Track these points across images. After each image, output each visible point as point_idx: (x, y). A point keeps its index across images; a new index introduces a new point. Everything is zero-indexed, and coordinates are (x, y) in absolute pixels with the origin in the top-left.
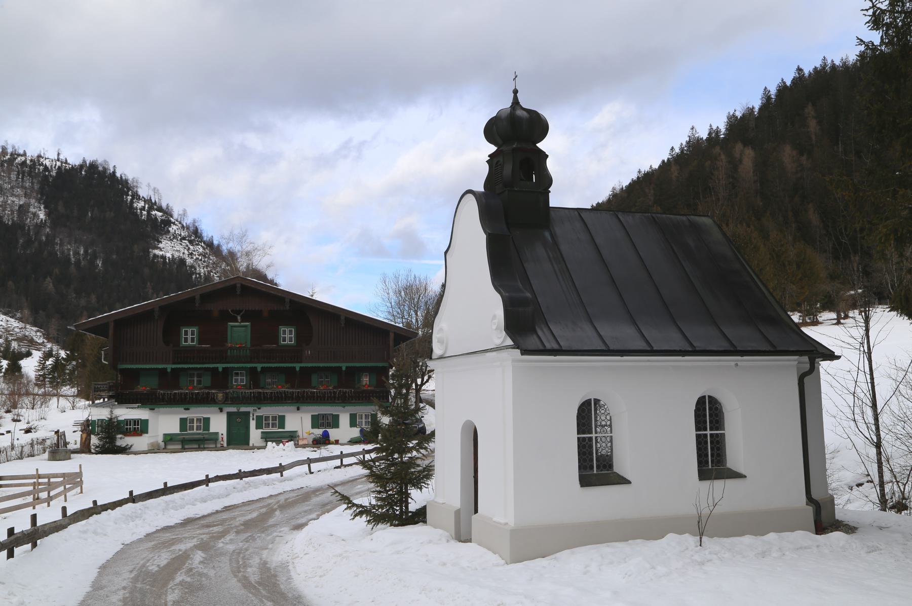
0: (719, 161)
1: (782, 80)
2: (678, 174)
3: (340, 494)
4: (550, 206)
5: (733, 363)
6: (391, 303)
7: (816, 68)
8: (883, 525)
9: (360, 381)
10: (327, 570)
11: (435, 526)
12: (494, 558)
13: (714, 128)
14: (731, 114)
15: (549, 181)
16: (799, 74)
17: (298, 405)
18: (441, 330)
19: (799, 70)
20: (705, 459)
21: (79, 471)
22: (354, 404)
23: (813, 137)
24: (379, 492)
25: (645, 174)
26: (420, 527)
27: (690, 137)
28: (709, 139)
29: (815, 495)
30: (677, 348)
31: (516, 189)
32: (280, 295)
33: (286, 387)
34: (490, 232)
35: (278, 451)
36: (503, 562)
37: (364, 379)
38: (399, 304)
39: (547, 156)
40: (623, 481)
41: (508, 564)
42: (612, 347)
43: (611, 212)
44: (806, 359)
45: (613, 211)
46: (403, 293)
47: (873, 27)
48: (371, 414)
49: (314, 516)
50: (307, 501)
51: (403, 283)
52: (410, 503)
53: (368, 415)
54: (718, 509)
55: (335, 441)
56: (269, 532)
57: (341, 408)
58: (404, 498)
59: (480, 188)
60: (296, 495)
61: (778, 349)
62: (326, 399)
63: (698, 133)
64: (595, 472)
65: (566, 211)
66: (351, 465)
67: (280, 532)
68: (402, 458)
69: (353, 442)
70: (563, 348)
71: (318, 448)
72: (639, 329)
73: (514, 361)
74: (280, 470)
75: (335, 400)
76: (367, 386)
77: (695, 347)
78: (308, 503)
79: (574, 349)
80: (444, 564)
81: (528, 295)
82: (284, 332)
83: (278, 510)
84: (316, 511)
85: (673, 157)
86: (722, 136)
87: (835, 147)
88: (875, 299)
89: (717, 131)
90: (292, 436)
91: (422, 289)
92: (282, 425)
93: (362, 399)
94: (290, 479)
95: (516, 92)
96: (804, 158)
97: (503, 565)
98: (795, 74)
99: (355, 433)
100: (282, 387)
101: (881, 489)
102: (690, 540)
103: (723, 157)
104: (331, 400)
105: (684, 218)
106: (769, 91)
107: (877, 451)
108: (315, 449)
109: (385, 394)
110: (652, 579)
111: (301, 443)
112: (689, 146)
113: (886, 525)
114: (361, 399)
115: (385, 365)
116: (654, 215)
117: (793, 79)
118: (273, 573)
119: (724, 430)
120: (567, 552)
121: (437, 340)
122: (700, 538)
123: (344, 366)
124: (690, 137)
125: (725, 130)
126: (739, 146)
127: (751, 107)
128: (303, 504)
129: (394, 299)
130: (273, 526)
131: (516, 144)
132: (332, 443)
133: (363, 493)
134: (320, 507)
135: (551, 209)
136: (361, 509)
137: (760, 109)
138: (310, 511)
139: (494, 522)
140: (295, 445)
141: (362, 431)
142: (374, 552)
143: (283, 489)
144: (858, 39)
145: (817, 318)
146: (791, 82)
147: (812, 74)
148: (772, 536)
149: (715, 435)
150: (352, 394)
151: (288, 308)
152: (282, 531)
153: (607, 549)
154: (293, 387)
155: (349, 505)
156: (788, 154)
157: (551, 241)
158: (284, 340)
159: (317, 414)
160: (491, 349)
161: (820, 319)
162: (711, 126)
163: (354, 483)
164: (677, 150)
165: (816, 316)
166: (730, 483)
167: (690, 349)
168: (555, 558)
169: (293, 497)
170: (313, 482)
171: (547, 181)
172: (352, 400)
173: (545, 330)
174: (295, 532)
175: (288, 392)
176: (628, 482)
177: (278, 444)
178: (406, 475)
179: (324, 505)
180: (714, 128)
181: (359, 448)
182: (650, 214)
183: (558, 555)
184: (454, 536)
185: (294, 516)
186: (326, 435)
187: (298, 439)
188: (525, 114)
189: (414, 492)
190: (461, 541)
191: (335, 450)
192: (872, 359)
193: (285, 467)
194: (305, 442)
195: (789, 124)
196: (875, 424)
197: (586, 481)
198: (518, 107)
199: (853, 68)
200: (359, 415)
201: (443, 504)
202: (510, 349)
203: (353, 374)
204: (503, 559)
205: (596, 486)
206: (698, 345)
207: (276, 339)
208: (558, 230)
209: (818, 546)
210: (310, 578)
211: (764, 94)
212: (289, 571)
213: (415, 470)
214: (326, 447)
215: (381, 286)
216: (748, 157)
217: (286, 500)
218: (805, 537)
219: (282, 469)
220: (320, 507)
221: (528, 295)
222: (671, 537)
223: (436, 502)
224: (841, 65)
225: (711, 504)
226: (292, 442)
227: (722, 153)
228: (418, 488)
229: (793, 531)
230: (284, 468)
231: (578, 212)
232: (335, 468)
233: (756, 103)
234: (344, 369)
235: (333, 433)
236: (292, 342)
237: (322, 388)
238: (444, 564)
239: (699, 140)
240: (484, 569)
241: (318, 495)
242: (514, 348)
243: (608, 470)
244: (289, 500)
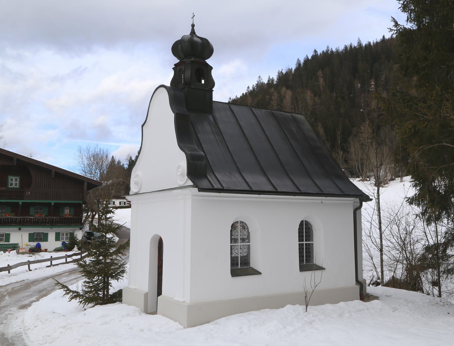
0: (273, 96)
1: (307, 56)
2: (252, 101)
3: (61, 284)
4: (213, 100)
5: (320, 201)
6: (84, 165)
7: (323, 51)
8: (388, 295)
9: (63, 212)
10: (55, 338)
11: (129, 305)
12: (176, 325)
13: (271, 78)
14: (280, 71)
15: (213, 84)
16: (315, 53)
17: (19, 227)
18: (137, 176)
19: (315, 51)
20: (302, 259)
22: (59, 226)
23: (321, 87)
24: (88, 283)
25: (233, 100)
26: (118, 305)
27: (258, 82)
28: (268, 84)
29: (360, 279)
30: (291, 191)
31: (192, 87)
32: (10, 155)
33: (12, 215)
34: (177, 112)
35: (5, 256)
36: (182, 327)
37: (66, 211)
38: (89, 165)
39: (212, 68)
40: (256, 273)
41: (185, 329)
42: (254, 189)
43: (248, 107)
44: (358, 200)
45: (249, 107)
46: (92, 159)
47: (403, 10)
48: (70, 233)
49: (34, 299)
50: (28, 289)
51: (92, 152)
52: (110, 289)
53: (68, 233)
54: (319, 288)
55: (45, 249)
56: (2, 311)
57: (49, 229)
58: (106, 285)
59: (168, 84)
60: (20, 285)
61: (345, 193)
62: (32, 222)
63: (262, 80)
64: (239, 267)
65: (221, 104)
66: (57, 265)
67: (10, 311)
68: (105, 260)
69: (57, 250)
70: (225, 188)
71: (33, 254)
72: (268, 178)
73: (193, 195)
74: (8, 269)
75: (46, 224)
76: (68, 215)
77: (301, 191)
78: (29, 290)
79: (231, 189)
80: (142, 330)
81: (202, 153)
82: (12, 180)
83: (7, 296)
84: (35, 296)
85: (249, 92)
86: (275, 83)
87: (332, 94)
88: (350, 175)
89: (273, 80)
90: (15, 247)
91: (105, 157)
92: (8, 239)
93: (65, 224)
94: (15, 275)
95: (193, 26)
96: (317, 98)
97: (182, 329)
98: (313, 53)
99: (59, 244)
100: (9, 215)
101: (382, 274)
102: (300, 308)
103: (275, 94)
104: (43, 224)
105: (289, 114)
106: (300, 61)
107: (381, 253)
108: (31, 255)
109: (80, 220)
110: (286, 335)
111: (20, 251)
112: (257, 87)
113: (390, 294)
114: (63, 223)
115: (81, 203)
116: (272, 111)
117: (312, 56)
118: (10, 342)
119: (313, 241)
120: (224, 319)
121: (134, 183)
122: (306, 307)
123: (53, 202)
124: (258, 82)
125: (276, 79)
126: (284, 89)
127: (291, 69)
128: (25, 291)
129: (86, 162)
130: (5, 307)
131: (193, 58)
132: (43, 251)
133: (67, 283)
134: (37, 292)
135: (213, 102)
136: (76, 294)
137: (295, 70)
138: (31, 296)
139: (175, 300)
140: (17, 252)
141: (64, 243)
142: (89, 323)
143: (10, 281)
144: (392, 18)
146: (311, 57)
147: (321, 54)
148: (342, 304)
149: (308, 244)
150: (57, 220)
151: (15, 164)
152: (12, 310)
153: (253, 315)
154: (16, 215)
155: (67, 292)
156: (309, 95)
157: (213, 120)
158: (11, 184)
159: (33, 232)
160: (176, 188)
162: (269, 77)
163: (60, 276)
164: (251, 88)
166: (318, 273)
167: (298, 192)
168: (217, 323)
169: (17, 287)
170: (31, 276)
171: (211, 84)
172: (58, 224)
173: (212, 176)
174: (22, 310)
175: (13, 218)
176: (260, 273)
177: (5, 252)
178: (108, 271)
179: (40, 291)
180: (271, 78)
181: (63, 254)
182: (270, 110)
183: (218, 321)
184: (143, 310)
185: (19, 300)
186: (39, 246)
187: (18, 248)
188: (199, 40)
189: (113, 282)
190: (147, 313)
191: (46, 256)
192: (380, 202)
193: (12, 267)
194: (24, 251)
195: (310, 79)
196: (380, 239)
197: (235, 273)
198: (194, 35)
199: (341, 53)
200: (62, 233)
201: (135, 289)
202: (191, 188)
203: (58, 208)
204: (181, 325)
206: (303, 189)
207: (5, 183)
208: (217, 115)
209: (368, 309)
210: (42, 344)
211: (297, 62)
212: (23, 340)
213: (115, 267)
214: (39, 254)
215: (77, 154)
216: (288, 94)
217: (13, 288)
218: (358, 303)
219: (10, 269)
220: (37, 292)
221: (202, 153)
222: (288, 307)
223: (129, 288)
224: (336, 51)
225: (313, 286)
226: (15, 251)
227: (275, 92)
228: (116, 279)
229: (352, 300)
230: (11, 268)
231: (229, 106)
232: (46, 267)
233: (293, 67)
234: (53, 204)
235: (44, 245)
236: (17, 186)
237: (37, 216)
238: (142, 330)
239: (263, 84)
240: (170, 333)
241: (35, 285)
242: (194, 187)
243: (247, 266)
244: (15, 289)
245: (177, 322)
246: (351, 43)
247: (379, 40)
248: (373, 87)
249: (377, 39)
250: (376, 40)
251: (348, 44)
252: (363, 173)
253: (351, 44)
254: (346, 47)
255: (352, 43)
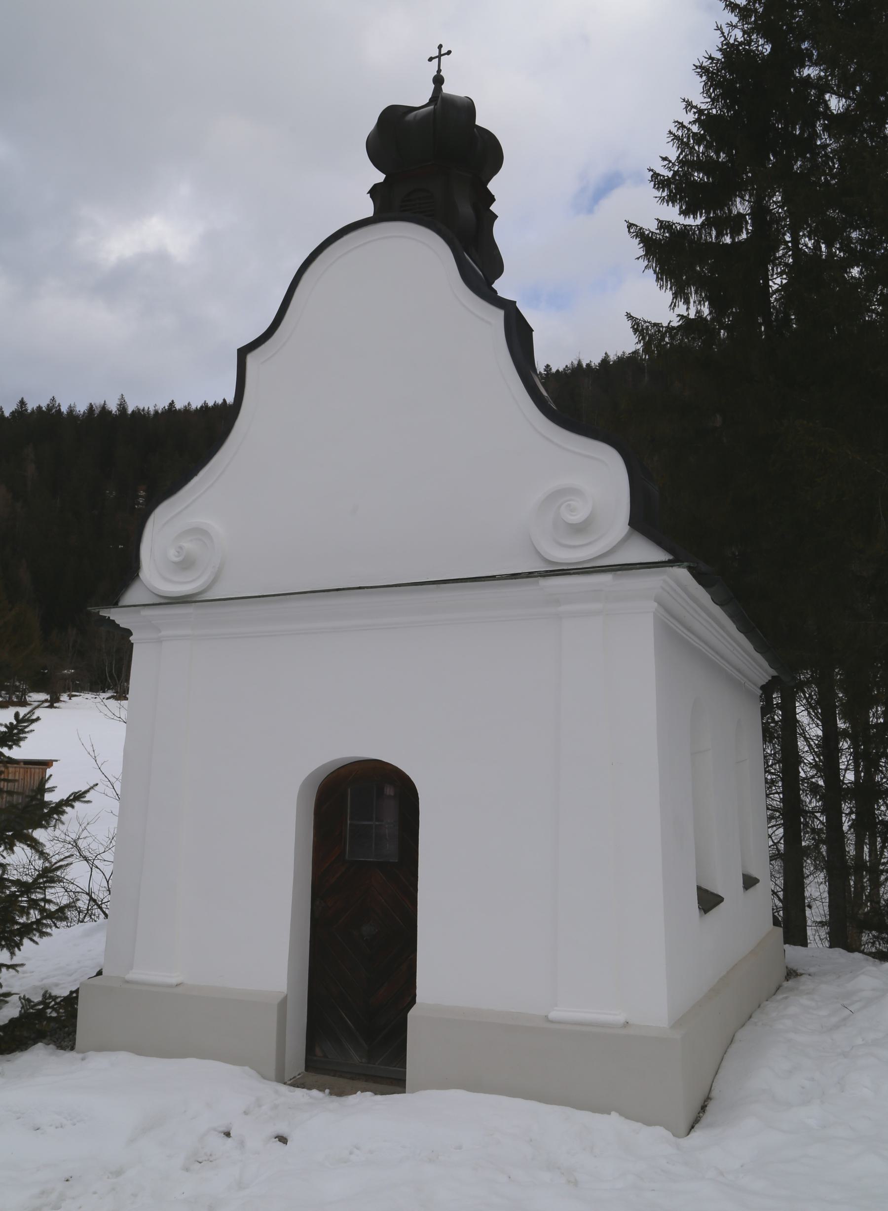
7: (39, 408)
16: (22, 407)
19: (22, 403)
21: (230, 400)
145: (25, 698)
161: (28, 699)
165: (25, 695)
205: (349, 764)
245: (613, 1113)
246: (105, 402)
247: (161, 409)
248: (141, 501)
249: (156, 405)
250: (155, 407)
251: (98, 402)
252: (119, 681)
253: (105, 404)
254: (91, 408)
255: (106, 403)
